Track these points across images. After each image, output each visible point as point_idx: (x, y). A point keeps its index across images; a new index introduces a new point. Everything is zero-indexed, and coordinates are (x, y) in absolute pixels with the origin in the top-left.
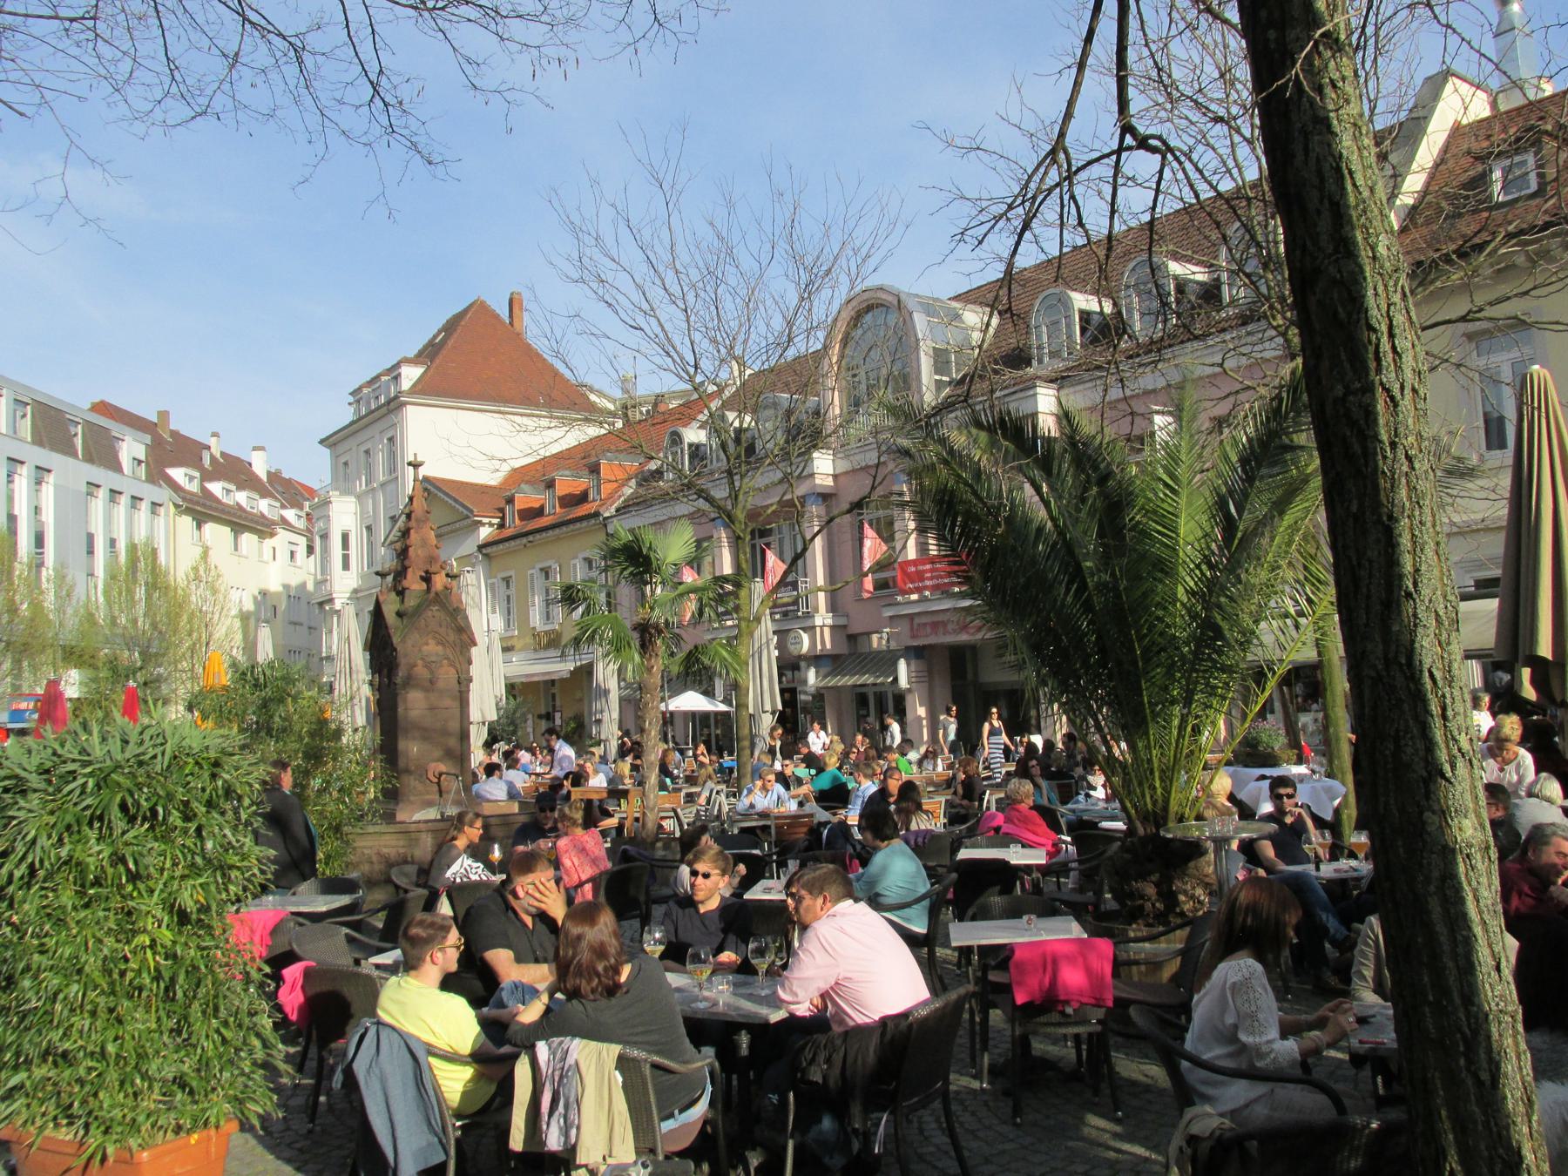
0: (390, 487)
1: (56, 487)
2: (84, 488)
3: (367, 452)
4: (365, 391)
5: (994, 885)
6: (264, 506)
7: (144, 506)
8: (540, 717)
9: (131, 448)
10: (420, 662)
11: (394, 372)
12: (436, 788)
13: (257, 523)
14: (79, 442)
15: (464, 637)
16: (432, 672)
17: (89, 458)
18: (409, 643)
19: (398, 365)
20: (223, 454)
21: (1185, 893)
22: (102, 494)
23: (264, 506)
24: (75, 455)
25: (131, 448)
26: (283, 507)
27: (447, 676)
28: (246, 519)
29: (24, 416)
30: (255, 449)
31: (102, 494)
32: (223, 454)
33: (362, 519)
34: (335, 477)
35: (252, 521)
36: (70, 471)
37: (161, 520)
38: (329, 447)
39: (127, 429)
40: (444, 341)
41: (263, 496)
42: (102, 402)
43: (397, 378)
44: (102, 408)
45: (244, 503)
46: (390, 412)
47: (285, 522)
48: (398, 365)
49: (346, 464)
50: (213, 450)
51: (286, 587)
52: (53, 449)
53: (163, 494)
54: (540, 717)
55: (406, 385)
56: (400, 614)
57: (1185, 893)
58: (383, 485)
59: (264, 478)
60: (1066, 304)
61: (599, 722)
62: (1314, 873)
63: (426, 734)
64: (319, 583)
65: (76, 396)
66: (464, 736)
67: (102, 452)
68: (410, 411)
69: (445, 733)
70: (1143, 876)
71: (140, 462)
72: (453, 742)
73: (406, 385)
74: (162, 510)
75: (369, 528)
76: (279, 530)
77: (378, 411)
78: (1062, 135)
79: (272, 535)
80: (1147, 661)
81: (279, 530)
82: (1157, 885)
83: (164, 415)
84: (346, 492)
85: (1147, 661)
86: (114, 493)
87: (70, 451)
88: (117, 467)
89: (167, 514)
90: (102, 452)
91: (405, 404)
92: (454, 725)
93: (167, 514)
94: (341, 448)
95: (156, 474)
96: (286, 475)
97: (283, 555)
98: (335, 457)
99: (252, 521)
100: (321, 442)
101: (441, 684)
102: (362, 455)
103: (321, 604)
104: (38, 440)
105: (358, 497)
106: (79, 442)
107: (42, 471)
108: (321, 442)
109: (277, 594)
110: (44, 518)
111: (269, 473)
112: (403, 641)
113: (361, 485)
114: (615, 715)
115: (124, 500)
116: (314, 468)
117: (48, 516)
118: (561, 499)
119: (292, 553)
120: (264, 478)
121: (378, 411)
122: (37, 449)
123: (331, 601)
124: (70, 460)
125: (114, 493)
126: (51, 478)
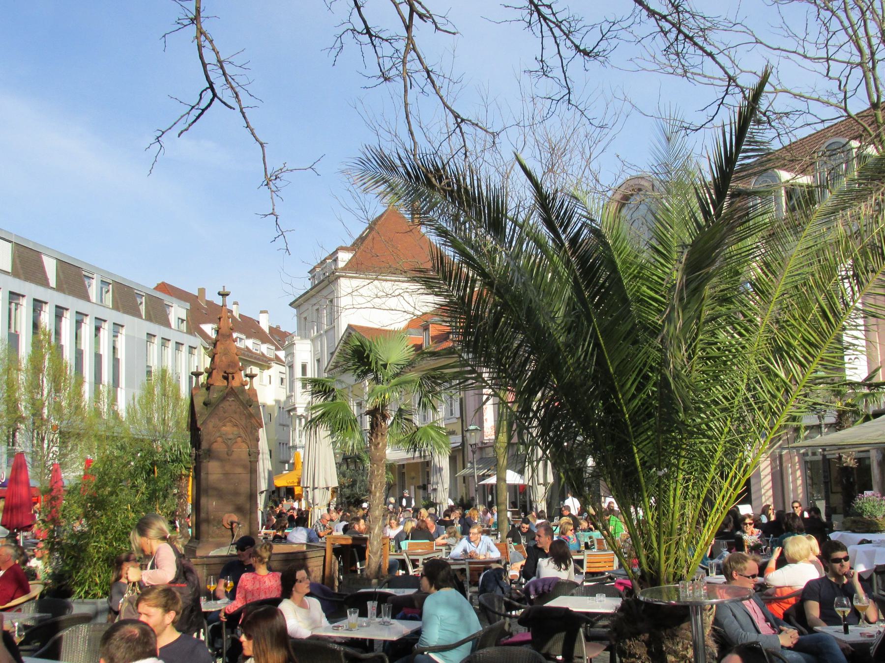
0: (331, 333)
1: (127, 336)
2: (145, 337)
3: (317, 310)
4: (318, 270)
5: (559, 631)
6: (265, 349)
7: (185, 349)
8: (419, 487)
9: (177, 312)
10: (219, 439)
11: (334, 256)
12: (230, 533)
13: (258, 359)
14: (143, 308)
15: (253, 421)
16: (228, 446)
17: (149, 318)
18: (210, 425)
19: (336, 252)
20: (240, 316)
21: (675, 653)
22: (157, 341)
23: (265, 349)
24: (140, 316)
25: (177, 312)
26: (277, 349)
27: (241, 450)
28: (251, 357)
29: (108, 291)
30: (262, 312)
31: (157, 341)
32: (240, 316)
33: (315, 355)
34: (299, 328)
35: (255, 358)
36: (136, 327)
37: (196, 357)
38: (295, 308)
39: (174, 299)
40: (367, 235)
41: (263, 342)
42: (163, 284)
43: (336, 260)
44: (164, 287)
45: (251, 346)
46: (330, 283)
47: (278, 360)
48: (336, 252)
49: (305, 318)
50: (234, 313)
51: (278, 402)
52: (124, 312)
53: (197, 341)
54: (419, 487)
55: (341, 264)
56: (205, 404)
57: (675, 653)
58: (326, 332)
59: (267, 330)
60: (776, 178)
61: (435, 490)
62: (843, 637)
63: (220, 494)
64: (289, 397)
65: (145, 280)
66: (252, 497)
67: (158, 314)
68: (343, 282)
69: (236, 493)
70: (635, 635)
71: (183, 321)
72: (242, 500)
73: (341, 264)
74: (196, 352)
75: (318, 361)
76: (273, 364)
77: (324, 282)
78: (761, 43)
79: (269, 367)
80: (636, 424)
81: (273, 364)
82: (648, 644)
83: (202, 291)
84: (304, 336)
85: (636, 424)
86: (165, 340)
87: (136, 313)
88: (167, 324)
89: (199, 354)
90: (158, 314)
91: (339, 277)
92: (244, 488)
93: (199, 354)
94: (303, 308)
95: (193, 328)
96: (283, 329)
97: (276, 380)
98: (299, 316)
99: (255, 358)
100: (291, 305)
101: (235, 456)
102: (315, 312)
103: (289, 411)
104: (116, 307)
105: (312, 340)
106: (143, 308)
107: (117, 326)
108: (291, 305)
109: (273, 407)
110: (119, 357)
111: (271, 328)
112: (204, 423)
113: (314, 333)
114: (447, 485)
115: (171, 345)
116: (288, 322)
117: (121, 355)
118: (433, 338)
119: (282, 379)
120: (267, 330)
121: (324, 282)
122: (115, 312)
123: (294, 409)
124: (136, 319)
125: (165, 340)
126: (123, 331)
